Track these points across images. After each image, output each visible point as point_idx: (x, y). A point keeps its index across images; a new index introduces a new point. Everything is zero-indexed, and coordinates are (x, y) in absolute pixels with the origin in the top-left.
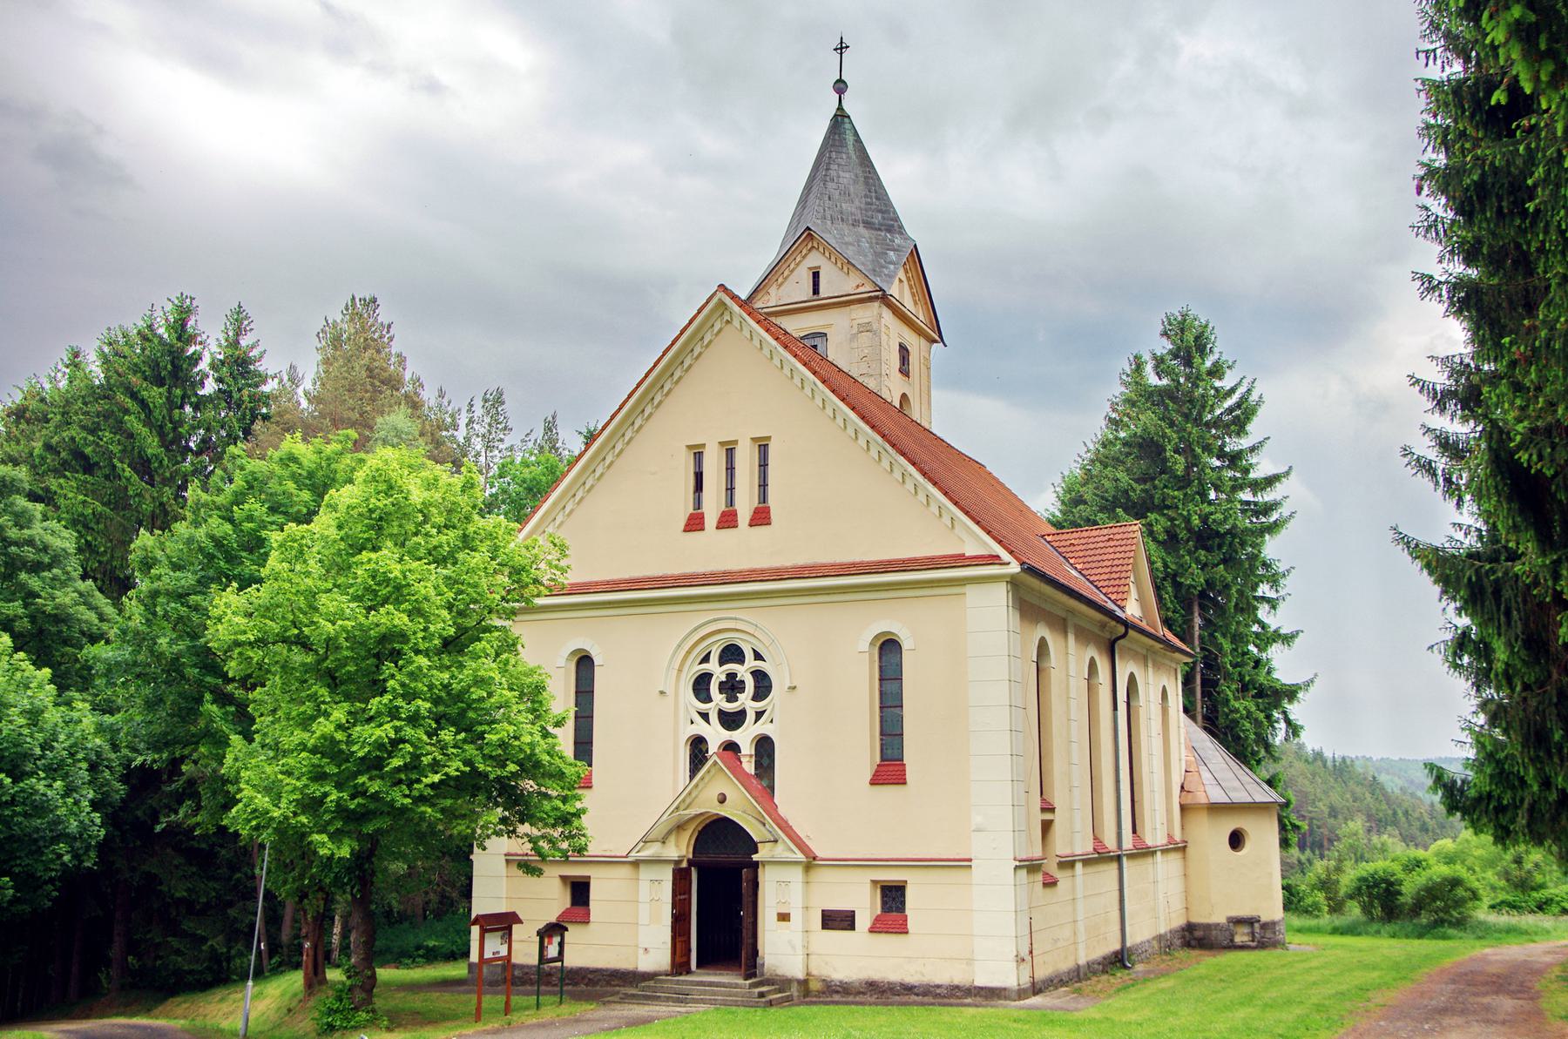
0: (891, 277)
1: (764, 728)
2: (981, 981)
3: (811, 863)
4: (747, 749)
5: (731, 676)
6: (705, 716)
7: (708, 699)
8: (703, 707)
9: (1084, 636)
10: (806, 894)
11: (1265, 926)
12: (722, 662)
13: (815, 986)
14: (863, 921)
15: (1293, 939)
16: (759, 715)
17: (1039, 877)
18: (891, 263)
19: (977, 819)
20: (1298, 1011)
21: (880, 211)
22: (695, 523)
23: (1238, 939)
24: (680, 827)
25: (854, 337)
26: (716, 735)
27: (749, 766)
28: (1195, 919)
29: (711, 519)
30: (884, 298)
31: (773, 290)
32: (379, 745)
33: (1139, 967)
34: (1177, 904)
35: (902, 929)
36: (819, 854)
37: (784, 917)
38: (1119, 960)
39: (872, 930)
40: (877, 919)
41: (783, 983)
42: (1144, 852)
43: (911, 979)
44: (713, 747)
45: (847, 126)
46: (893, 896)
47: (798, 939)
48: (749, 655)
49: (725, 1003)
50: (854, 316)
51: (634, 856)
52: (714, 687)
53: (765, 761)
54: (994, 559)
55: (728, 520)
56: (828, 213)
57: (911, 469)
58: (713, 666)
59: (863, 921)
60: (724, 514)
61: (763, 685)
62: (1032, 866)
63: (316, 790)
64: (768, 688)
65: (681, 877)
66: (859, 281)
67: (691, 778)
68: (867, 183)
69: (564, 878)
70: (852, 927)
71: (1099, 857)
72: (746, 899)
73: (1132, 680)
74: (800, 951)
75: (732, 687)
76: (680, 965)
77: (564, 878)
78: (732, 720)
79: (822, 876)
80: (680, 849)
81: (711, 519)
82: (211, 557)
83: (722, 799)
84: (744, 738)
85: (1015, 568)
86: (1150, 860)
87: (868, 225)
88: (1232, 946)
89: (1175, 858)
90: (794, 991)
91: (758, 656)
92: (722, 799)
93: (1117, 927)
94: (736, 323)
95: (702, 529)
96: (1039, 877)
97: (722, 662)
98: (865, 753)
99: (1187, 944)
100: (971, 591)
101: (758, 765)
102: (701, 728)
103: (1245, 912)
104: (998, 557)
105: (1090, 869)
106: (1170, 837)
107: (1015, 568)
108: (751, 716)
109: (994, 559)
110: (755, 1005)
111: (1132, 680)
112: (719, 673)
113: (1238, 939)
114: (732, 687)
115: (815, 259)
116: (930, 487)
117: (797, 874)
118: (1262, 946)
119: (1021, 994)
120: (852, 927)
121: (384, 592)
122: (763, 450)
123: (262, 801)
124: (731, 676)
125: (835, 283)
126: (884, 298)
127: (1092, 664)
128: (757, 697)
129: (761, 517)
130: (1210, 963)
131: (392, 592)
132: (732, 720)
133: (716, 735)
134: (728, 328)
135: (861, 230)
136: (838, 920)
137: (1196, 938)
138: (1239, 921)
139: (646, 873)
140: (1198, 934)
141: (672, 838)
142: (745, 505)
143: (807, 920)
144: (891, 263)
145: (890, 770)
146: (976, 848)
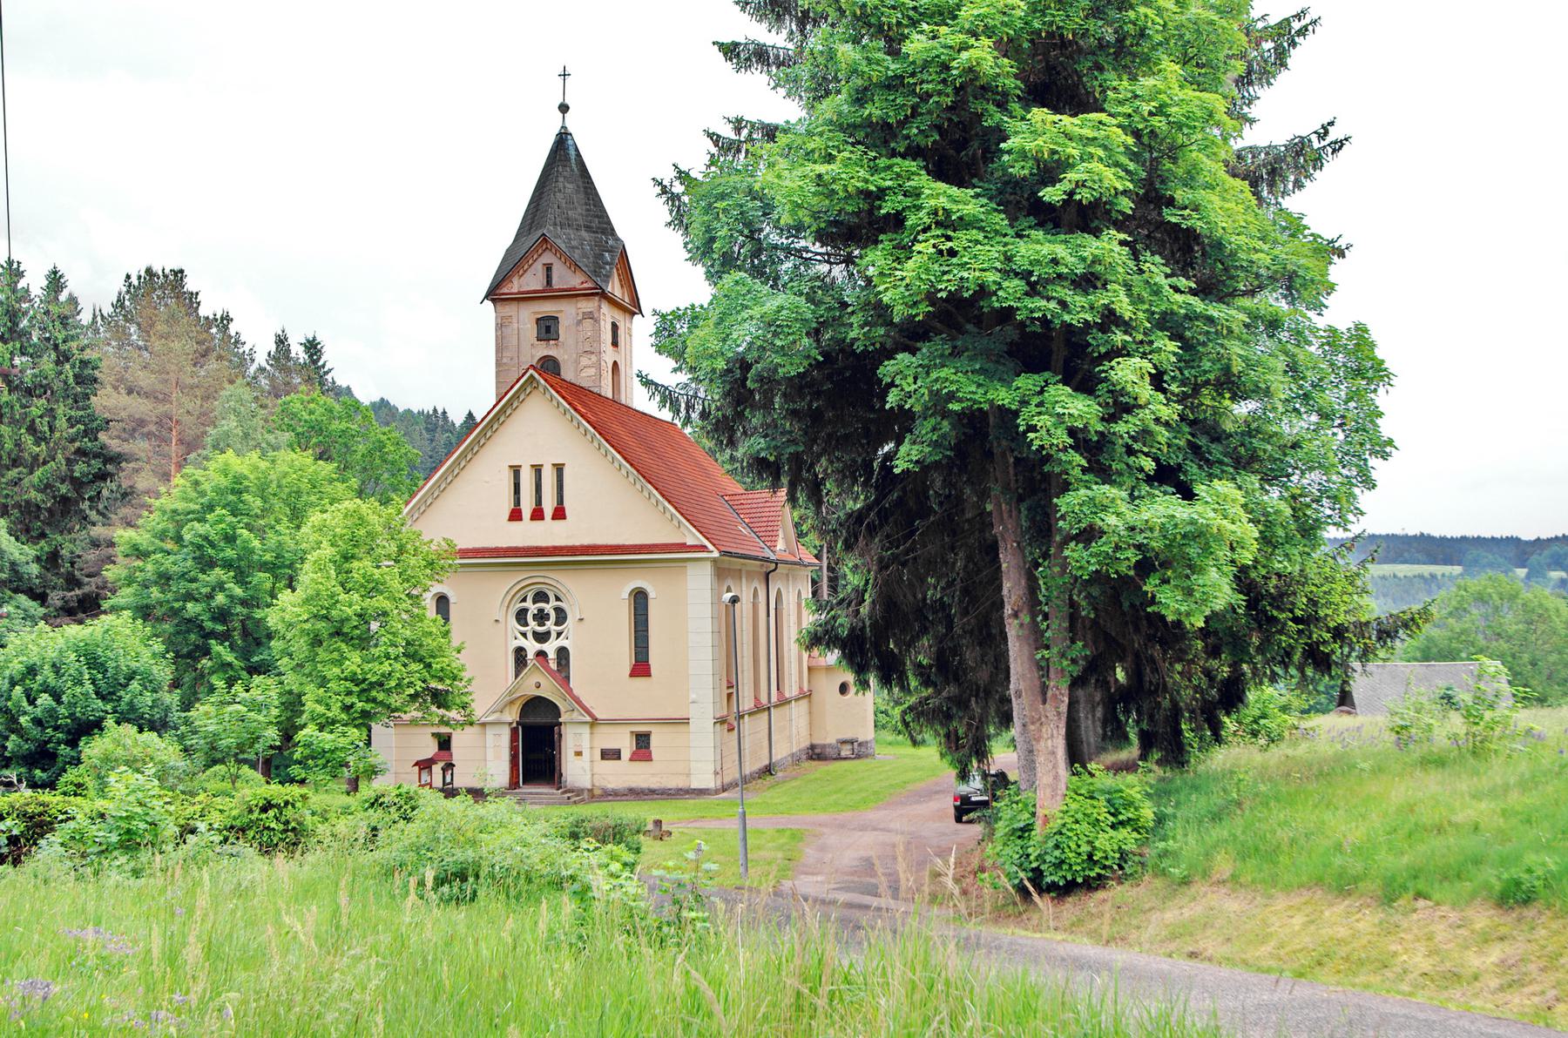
0: (608, 277)
1: (561, 642)
2: (695, 785)
3: (595, 722)
4: (552, 655)
5: (541, 610)
6: (524, 635)
7: (526, 625)
8: (523, 629)
9: (750, 576)
10: (591, 740)
11: (860, 745)
12: (534, 602)
13: (597, 792)
14: (626, 754)
15: (879, 750)
16: (559, 634)
17: (726, 726)
18: (607, 263)
19: (693, 696)
20: (863, 795)
21: (597, 216)
22: (516, 515)
23: (843, 754)
24: (512, 702)
25: (579, 322)
26: (532, 647)
27: (553, 666)
28: (815, 742)
29: (526, 513)
30: (603, 295)
31: (515, 280)
32: (383, 675)
33: (780, 774)
34: (804, 732)
35: (648, 758)
36: (598, 716)
37: (579, 754)
38: (768, 770)
39: (631, 760)
40: (634, 754)
41: (579, 792)
42: (783, 702)
43: (654, 786)
44: (530, 655)
45: (570, 142)
46: (643, 740)
47: (587, 766)
48: (552, 598)
49: (547, 804)
50: (579, 305)
51: (483, 720)
52: (530, 617)
53: (563, 662)
54: (703, 548)
55: (538, 515)
56: (558, 220)
57: (655, 492)
58: (529, 604)
59: (626, 754)
60: (534, 511)
61: (561, 616)
62: (722, 721)
63: (348, 701)
64: (565, 618)
65: (514, 732)
66: (583, 279)
67: (516, 677)
68: (586, 193)
69: (433, 734)
70: (619, 758)
71: (759, 709)
72: (557, 744)
73: (779, 593)
74: (589, 773)
75: (541, 617)
76: (514, 784)
77: (433, 734)
78: (542, 637)
79: (602, 730)
80: (512, 715)
81: (526, 513)
82: (200, 547)
83: (538, 686)
84: (550, 647)
85: (716, 554)
86: (787, 706)
87: (588, 228)
88: (839, 758)
89: (804, 704)
90: (586, 795)
91: (558, 599)
92: (538, 686)
93: (767, 750)
94: (541, 389)
95: (521, 520)
96: (726, 726)
97: (534, 602)
98: (626, 659)
99: (811, 758)
100: (689, 565)
101: (559, 664)
102: (522, 642)
103: (848, 736)
104: (705, 547)
105: (753, 717)
106: (801, 689)
107: (716, 554)
108: (554, 635)
109: (703, 548)
110: (568, 804)
111: (779, 593)
112: (533, 608)
113: (843, 754)
114: (541, 617)
115: (548, 258)
116: (666, 504)
117: (586, 730)
118: (859, 757)
119: (717, 792)
120: (619, 758)
121: (371, 585)
122: (559, 469)
123: (320, 709)
124: (541, 610)
125: (565, 278)
126: (603, 295)
127: (756, 590)
128: (557, 624)
129: (559, 514)
130: (823, 768)
131: (372, 588)
132: (542, 637)
133: (532, 647)
134: (535, 392)
135: (584, 234)
136: (611, 755)
137: (816, 754)
138: (844, 742)
139: (490, 731)
140: (818, 751)
141: (507, 709)
142: (548, 506)
143: (591, 754)
144: (607, 263)
145: (641, 668)
146: (692, 712)
